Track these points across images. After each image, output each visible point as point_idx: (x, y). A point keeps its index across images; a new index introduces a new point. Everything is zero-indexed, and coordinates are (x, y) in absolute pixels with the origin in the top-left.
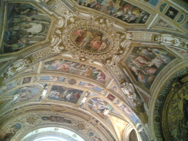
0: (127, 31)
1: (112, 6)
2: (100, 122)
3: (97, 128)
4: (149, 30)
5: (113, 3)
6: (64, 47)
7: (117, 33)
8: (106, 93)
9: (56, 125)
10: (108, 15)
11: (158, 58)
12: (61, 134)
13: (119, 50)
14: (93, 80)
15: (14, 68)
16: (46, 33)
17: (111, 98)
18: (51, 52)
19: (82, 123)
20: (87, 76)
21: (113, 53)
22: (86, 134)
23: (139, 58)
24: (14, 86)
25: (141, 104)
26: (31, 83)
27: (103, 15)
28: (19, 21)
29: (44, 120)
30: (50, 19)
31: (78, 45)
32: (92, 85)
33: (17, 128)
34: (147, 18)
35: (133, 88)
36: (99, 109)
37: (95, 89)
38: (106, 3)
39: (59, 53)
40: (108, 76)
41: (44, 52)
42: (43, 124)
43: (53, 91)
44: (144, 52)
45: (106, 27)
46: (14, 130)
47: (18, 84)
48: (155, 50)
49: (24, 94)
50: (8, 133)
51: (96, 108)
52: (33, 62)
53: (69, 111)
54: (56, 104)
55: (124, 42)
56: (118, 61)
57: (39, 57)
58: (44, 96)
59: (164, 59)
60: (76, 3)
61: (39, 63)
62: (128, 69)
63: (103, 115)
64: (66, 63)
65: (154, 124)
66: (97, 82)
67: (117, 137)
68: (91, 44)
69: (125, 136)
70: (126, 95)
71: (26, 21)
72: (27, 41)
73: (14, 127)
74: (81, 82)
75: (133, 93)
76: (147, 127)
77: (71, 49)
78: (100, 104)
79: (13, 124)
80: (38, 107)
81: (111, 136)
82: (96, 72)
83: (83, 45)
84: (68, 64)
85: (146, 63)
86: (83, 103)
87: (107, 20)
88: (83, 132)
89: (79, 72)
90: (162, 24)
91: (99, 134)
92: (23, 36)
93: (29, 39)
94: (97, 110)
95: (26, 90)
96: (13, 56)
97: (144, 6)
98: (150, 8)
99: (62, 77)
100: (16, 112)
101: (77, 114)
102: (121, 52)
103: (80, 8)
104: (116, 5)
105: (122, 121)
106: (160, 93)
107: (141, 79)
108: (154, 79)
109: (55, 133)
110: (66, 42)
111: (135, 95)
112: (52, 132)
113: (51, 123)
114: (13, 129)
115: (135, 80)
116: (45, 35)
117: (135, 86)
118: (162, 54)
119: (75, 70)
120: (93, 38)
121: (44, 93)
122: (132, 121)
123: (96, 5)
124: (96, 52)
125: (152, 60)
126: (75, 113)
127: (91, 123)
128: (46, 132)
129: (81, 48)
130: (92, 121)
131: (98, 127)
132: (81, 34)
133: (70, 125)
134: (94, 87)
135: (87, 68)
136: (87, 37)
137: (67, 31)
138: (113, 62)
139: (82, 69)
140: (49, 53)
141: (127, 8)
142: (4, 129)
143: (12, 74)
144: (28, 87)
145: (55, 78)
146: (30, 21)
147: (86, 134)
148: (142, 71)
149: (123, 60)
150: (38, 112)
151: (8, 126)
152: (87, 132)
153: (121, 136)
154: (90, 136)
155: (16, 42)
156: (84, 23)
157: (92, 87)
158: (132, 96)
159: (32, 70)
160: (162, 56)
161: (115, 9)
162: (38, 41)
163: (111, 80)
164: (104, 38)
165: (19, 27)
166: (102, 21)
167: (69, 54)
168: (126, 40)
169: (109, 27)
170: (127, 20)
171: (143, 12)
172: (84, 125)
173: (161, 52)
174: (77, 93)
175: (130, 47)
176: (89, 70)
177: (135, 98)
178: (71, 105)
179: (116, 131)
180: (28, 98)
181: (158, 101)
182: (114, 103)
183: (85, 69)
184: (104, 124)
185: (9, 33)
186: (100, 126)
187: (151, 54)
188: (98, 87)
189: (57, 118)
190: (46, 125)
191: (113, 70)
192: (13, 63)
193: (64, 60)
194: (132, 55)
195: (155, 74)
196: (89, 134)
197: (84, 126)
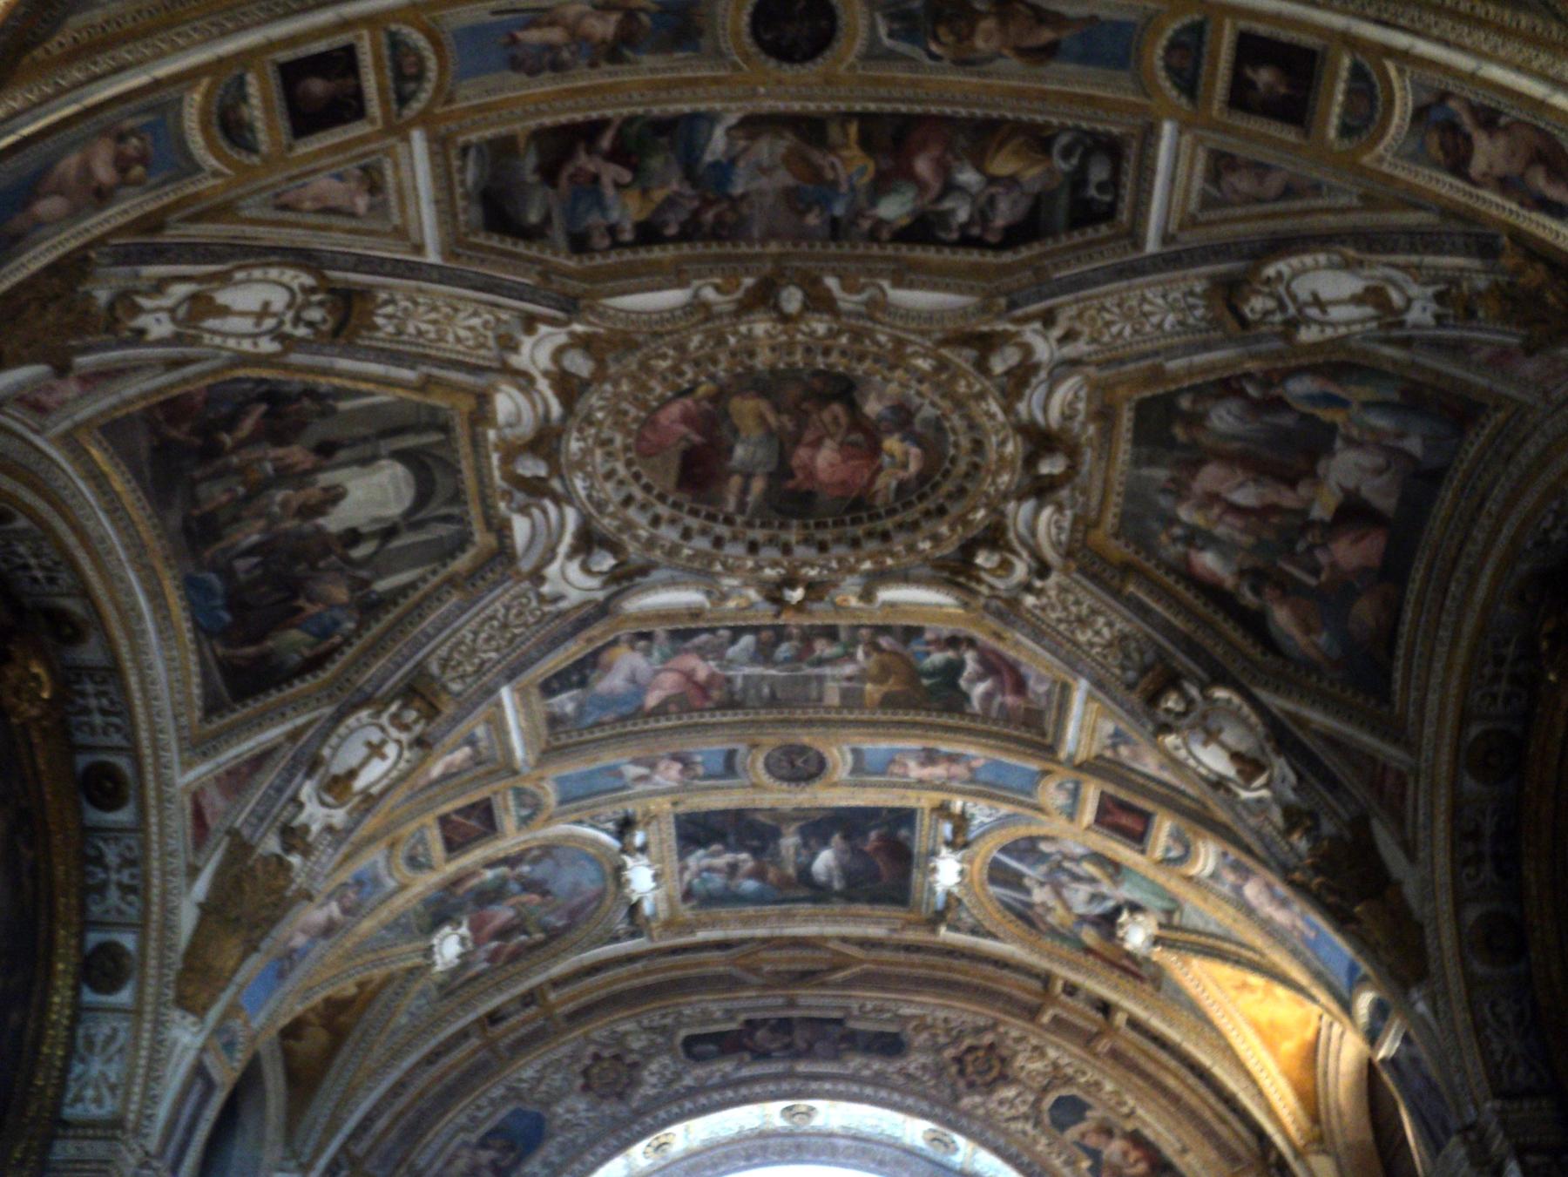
0: (1013, 305)
1: (816, 175)
3: (1116, 1055)
4: (1170, 261)
5: (816, 156)
6: (614, 547)
7: (945, 342)
8: (1075, 794)
9: (786, 1086)
10: (818, 247)
11: (1351, 442)
12: (842, 1142)
13: (1031, 461)
14: (945, 720)
15: (336, 780)
16: (457, 497)
17: (1126, 820)
18: (547, 608)
19: (988, 1038)
20: (888, 702)
21: (992, 490)
23: (1210, 477)
24: (391, 884)
25: (1348, 835)
26: (511, 839)
27: (781, 256)
28: (241, 490)
30: (434, 410)
31: (712, 509)
32: (952, 758)
33: (512, 1148)
34: (1116, 171)
35: (1254, 719)
36: (1083, 919)
37: (982, 776)
38: (764, 171)
39: (600, 596)
40: (1037, 663)
41: (495, 623)
42: (691, 1092)
43: (700, 852)
44: (1224, 418)
45: (840, 333)
47: (415, 863)
48: (1298, 387)
49: (502, 914)
51: (1060, 911)
52: (448, 709)
53: (875, 962)
54: (761, 932)
55: (1036, 395)
56: (1063, 537)
57: (477, 661)
58: (650, 896)
59: (1401, 435)
60: (548, 255)
61: (493, 699)
62: (1170, 580)
63: (1129, 955)
64: (687, 651)
65: (1471, 982)
66: (981, 726)
68: (800, 476)
70: (1218, 783)
71: (286, 475)
72: (352, 590)
73: (499, 1143)
74: (856, 752)
75: (1263, 760)
76: (1421, 1017)
77: (673, 551)
78: (1077, 878)
80: (647, 972)
81: (1230, 1101)
82: (938, 658)
83: (750, 499)
84: (702, 653)
85: (1288, 499)
86: (949, 894)
87: (832, 282)
88: (1001, 1103)
89: (814, 685)
90: (1242, 182)
91: (1131, 1102)
92: (313, 566)
93: (364, 573)
94: (1070, 921)
95: (502, 884)
96: (298, 704)
97: (1043, 96)
98: (1090, 100)
99: (707, 749)
100: (505, 1035)
101: (940, 974)
102: (1050, 467)
103: (593, 276)
104: (843, 160)
106: (1464, 719)
107: (1295, 632)
108: (1394, 612)
109: (804, 1140)
110: (613, 516)
111: (1280, 766)
112: (776, 1134)
113: (745, 1072)
114: (486, 1156)
115: (1256, 653)
116: (456, 510)
117: (1264, 695)
118: (1367, 405)
119: (773, 677)
120: (790, 425)
121: (641, 878)
122: (1318, 976)
123: (696, 213)
124: (864, 515)
125: (1321, 467)
126: (922, 972)
127: (1059, 1024)
128: (732, 1141)
129: (739, 519)
130: (1064, 1006)
131: (1121, 1045)
132: (699, 432)
133: (892, 1067)
134: (971, 770)
135: (854, 642)
136: (743, 435)
137: (582, 444)
138: (1025, 554)
139: (821, 662)
140: (531, 620)
141: (935, 151)
142: (430, 1164)
143: (339, 816)
144: (511, 861)
145: (662, 766)
146: (308, 465)
147: (1026, 1117)
148: (1281, 570)
149: (1096, 524)
152: (1031, 1098)
154: (1061, 1126)
155: (288, 615)
156: (671, 352)
157: (959, 770)
158: (1261, 780)
159: (477, 752)
160: (1381, 422)
161: (844, 188)
162: (428, 568)
163: (1065, 689)
164: (873, 407)
165: (261, 523)
166: (792, 299)
167: (672, 584)
168: (1043, 374)
169: (869, 324)
170: (975, 231)
171: (1064, 139)
172: (1005, 1052)
173: (1360, 393)
174: (873, 835)
175: (1105, 415)
176: (875, 656)
177: (1290, 796)
178: (878, 922)
179: (1251, 1065)
180: (544, 929)
181: (1469, 783)
182: (1158, 854)
183: (849, 657)
184: (1157, 1024)
185: (213, 579)
186: (1133, 1035)
187: (1287, 420)
188: (998, 764)
190: (716, 1097)
191: (1054, 616)
192: (319, 748)
193: (660, 631)
194: (1151, 462)
195: (1393, 570)
196: (1046, 1119)
197: (1003, 1060)
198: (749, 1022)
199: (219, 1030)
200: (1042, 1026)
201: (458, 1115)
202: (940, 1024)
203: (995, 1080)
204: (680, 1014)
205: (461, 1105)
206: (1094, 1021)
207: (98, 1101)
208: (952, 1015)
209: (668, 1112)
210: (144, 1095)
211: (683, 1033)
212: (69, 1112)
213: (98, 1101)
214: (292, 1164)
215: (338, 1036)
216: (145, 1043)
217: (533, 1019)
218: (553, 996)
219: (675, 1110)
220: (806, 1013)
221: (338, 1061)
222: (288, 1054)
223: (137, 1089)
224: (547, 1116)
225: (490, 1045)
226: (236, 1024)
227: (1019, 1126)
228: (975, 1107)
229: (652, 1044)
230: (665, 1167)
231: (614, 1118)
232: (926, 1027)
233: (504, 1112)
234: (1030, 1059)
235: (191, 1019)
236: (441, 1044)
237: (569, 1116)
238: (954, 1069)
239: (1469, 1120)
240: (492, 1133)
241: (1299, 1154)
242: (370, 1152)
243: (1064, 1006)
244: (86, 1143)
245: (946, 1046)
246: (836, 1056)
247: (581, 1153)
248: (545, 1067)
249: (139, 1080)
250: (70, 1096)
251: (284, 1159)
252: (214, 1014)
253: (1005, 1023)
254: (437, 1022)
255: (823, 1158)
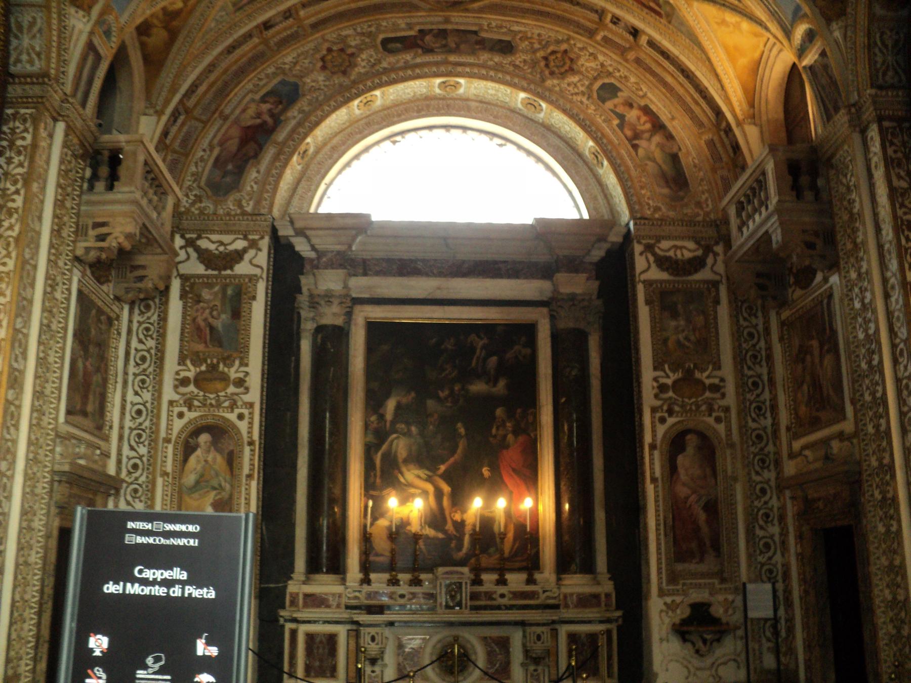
2: (649, 36)
3: (638, 61)
9: (443, 69)
12: (473, 104)
19: (564, 46)
22: (583, 93)
29: (391, 52)
33: (281, 103)
42: (386, 71)
46: (270, 111)
50: (249, 123)
67: (727, 100)
69: (764, 87)
73: (271, 100)
79: (265, 85)
91: (645, 89)
105: (746, 25)
109: (449, 102)
112: (435, 98)
113: (419, 60)
114: (265, 107)
122: (773, 14)
128: (410, 101)
130: (610, 30)
131: (642, 56)
133: (506, 60)
147: (583, 93)
150: (364, 24)
151: (247, 99)
152: (587, 83)
153: (745, 90)
154: (603, 100)
172: (573, 56)
179: (719, 70)
184: (666, 44)
189: (445, 38)
190: (401, 74)
196: (595, 95)
197: (572, 60)
198: (421, 31)
199: (100, 21)
200: (597, 42)
201: (247, 84)
202: (535, 36)
203: (566, 71)
204: (380, 25)
205: (249, 78)
206: (627, 40)
207: (31, 62)
208: (543, 32)
209: (373, 82)
210: (58, 61)
211: (381, 36)
212: (12, 69)
213: (31, 62)
214: (151, 111)
215: (173, 35)
216: (55, 27)
217: (291, 27)
218: (302, 13)
219: (377, 81)
220: (456, 27)
221: (174, 49)
222: (143, 45)
223: (54, 55)
224: (300, 84)
225: (265, 42)
226: (111, 18)
227: (579, 98)
228: (554, 86)
229: (363, 42)
230: (369, 116)
231: (341, 85)
232: (527, 38)
233: (275, 81)
234: (587, 60)
235: (81, 13)
236: (235, 41)
237: (314, 84)
238: (543, 64)
239: (852, 101)
240: (267, 94)
241: (739, 124)
242: (195, 106)
243: (610, 30)
244: (27, 87)
245: (539, 49)
246: (473, 53)
247: (321, 105)
248: (299, 55)
249: (54, 50)
250: (12, 60)
251: (146, 108)
252: (96, 11)
253: (574, 39)
254: (233, 26)
255: (462, 112)
